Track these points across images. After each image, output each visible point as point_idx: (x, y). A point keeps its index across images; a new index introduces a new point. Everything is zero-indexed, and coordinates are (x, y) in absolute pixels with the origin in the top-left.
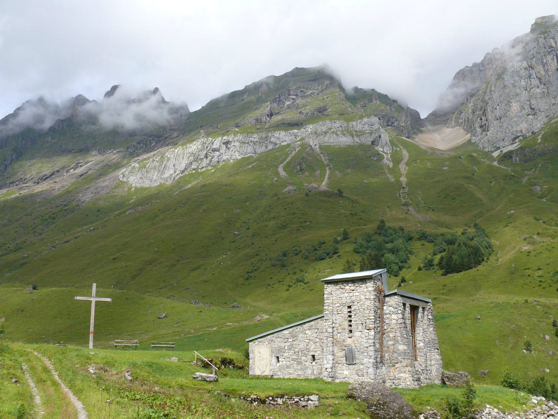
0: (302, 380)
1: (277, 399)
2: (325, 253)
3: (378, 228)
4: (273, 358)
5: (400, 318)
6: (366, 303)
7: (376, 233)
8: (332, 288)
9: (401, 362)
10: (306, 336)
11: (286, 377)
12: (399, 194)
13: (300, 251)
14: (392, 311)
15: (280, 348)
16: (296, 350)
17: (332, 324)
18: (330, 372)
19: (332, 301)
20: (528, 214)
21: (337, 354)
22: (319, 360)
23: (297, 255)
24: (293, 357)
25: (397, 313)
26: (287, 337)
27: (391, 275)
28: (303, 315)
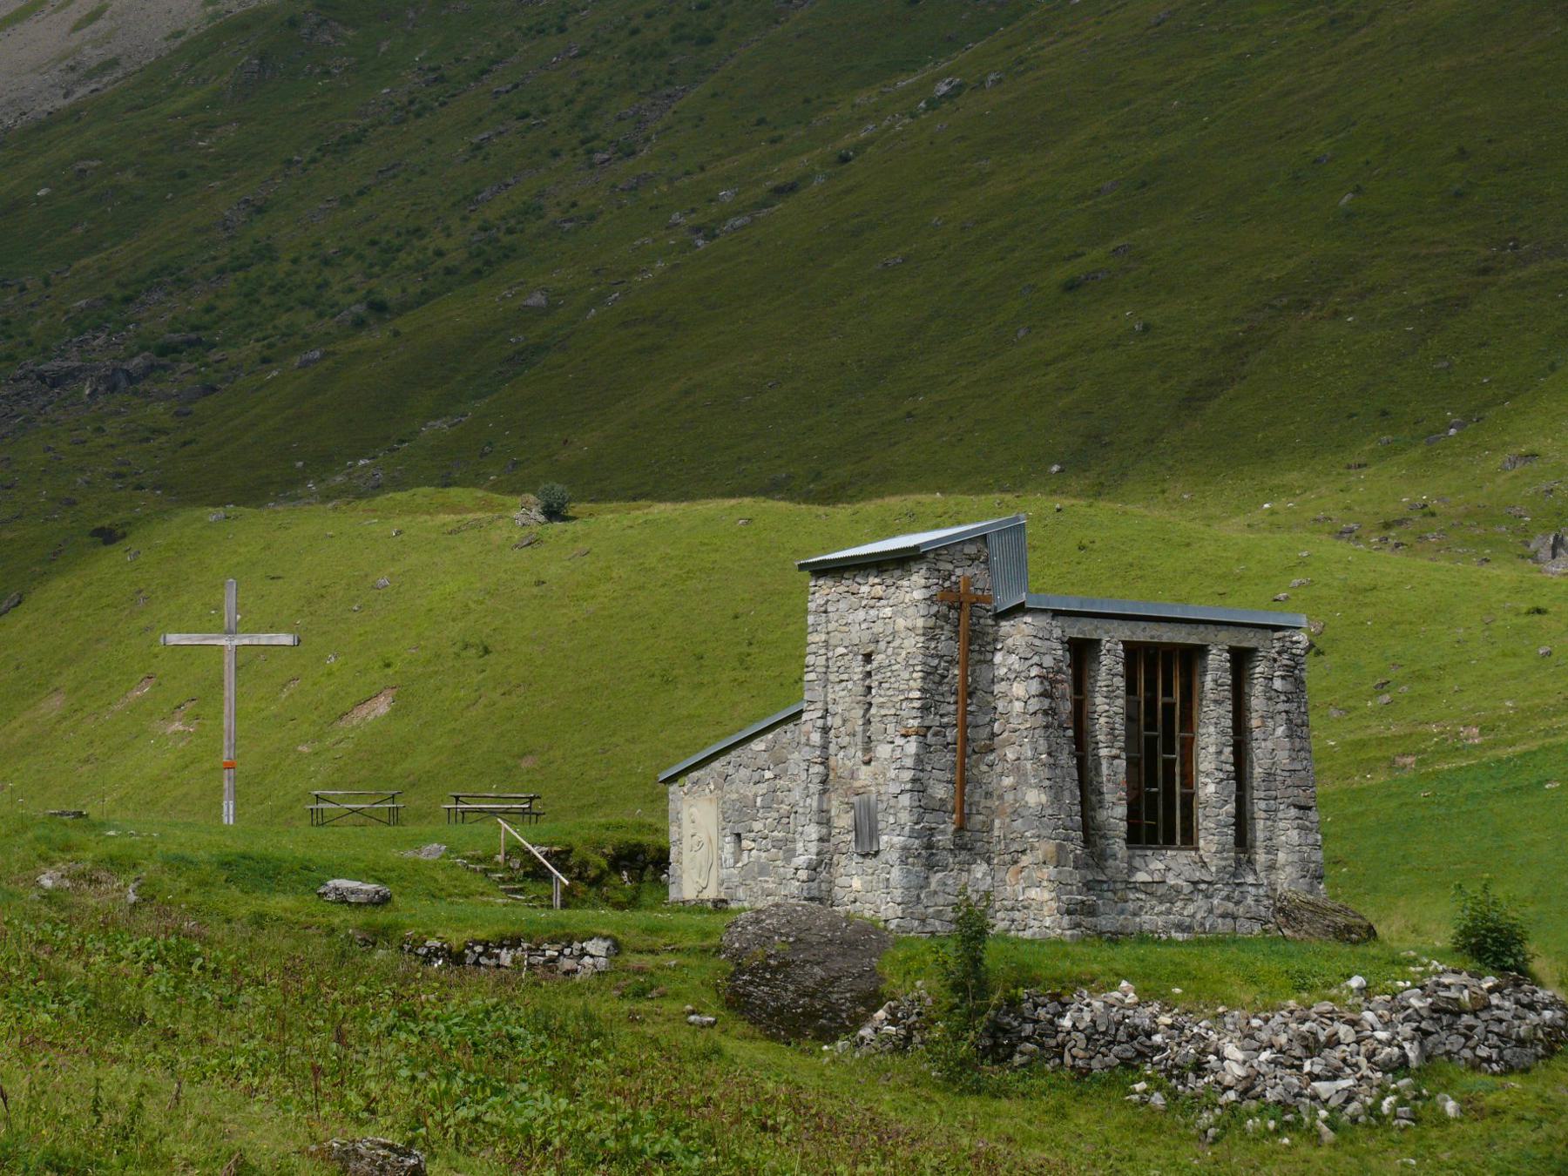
1: (497, 951)
4: (727, 839)
19: (823, 637)
24: (776, 833)
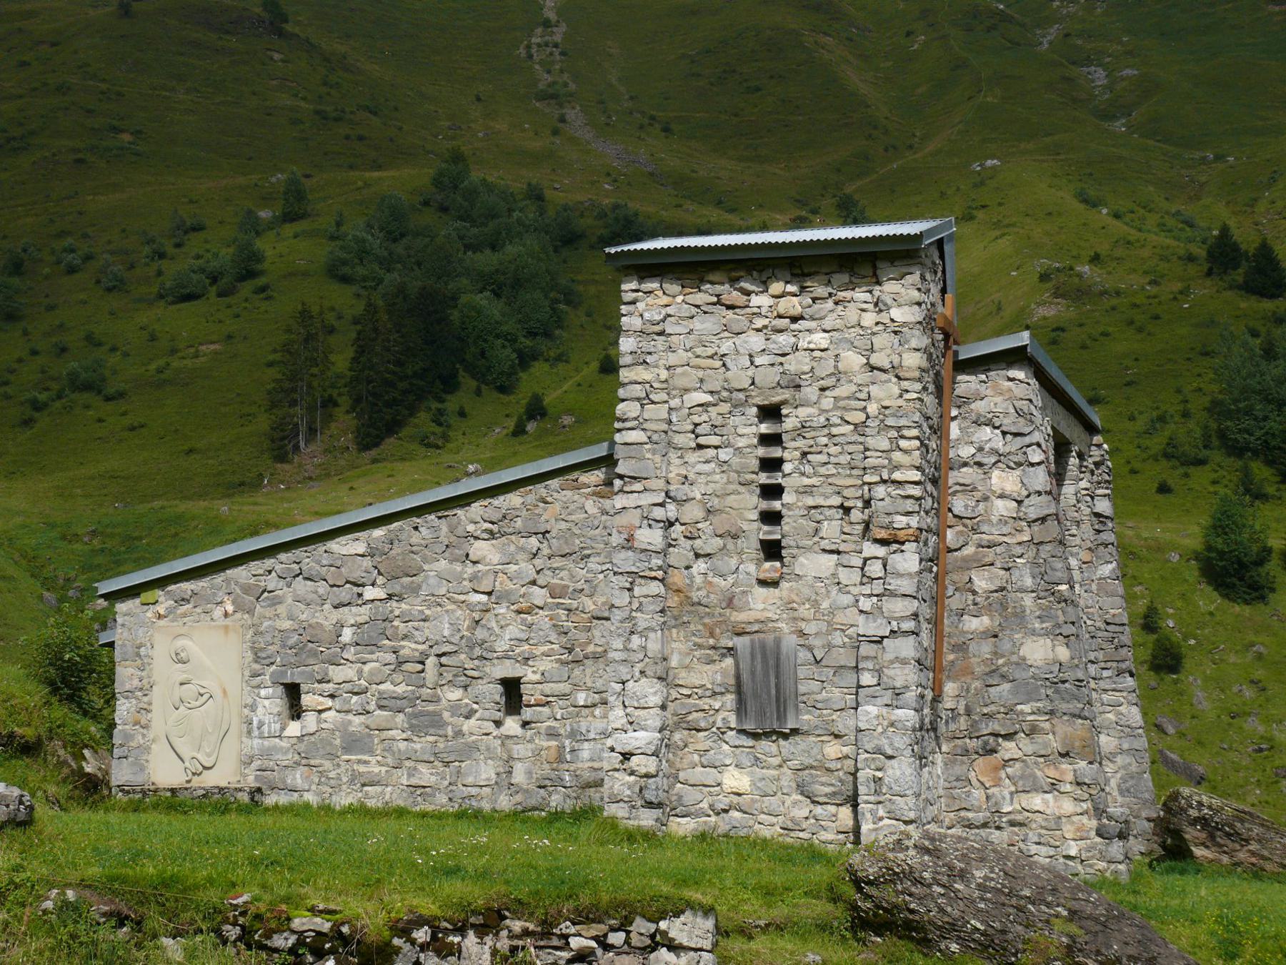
0: (440, 816)
1: (457, 939)
2: (202, 270)
3: (437, 182)
4: (263, 692)
5: (1039, 488)
6: (874, 390)
7: (426, 203)
8: (665, 300)
9: (1033, 731)
10: (470, 569)
11: (344, 799)
12: (528, 47)
13: (88, 258)
14: (994, 451)
15: (306, 637)
16: (409, 648)
17: (662, 505)
18: (647, 776)
19: (664, 374)
20: (1055, 176)
21: (683, 674)
22: (546, 710)
23: (72, 270)
25: (1019, 464)
26: (356, 575)
27: (483, 387)
28: (102, 533)
